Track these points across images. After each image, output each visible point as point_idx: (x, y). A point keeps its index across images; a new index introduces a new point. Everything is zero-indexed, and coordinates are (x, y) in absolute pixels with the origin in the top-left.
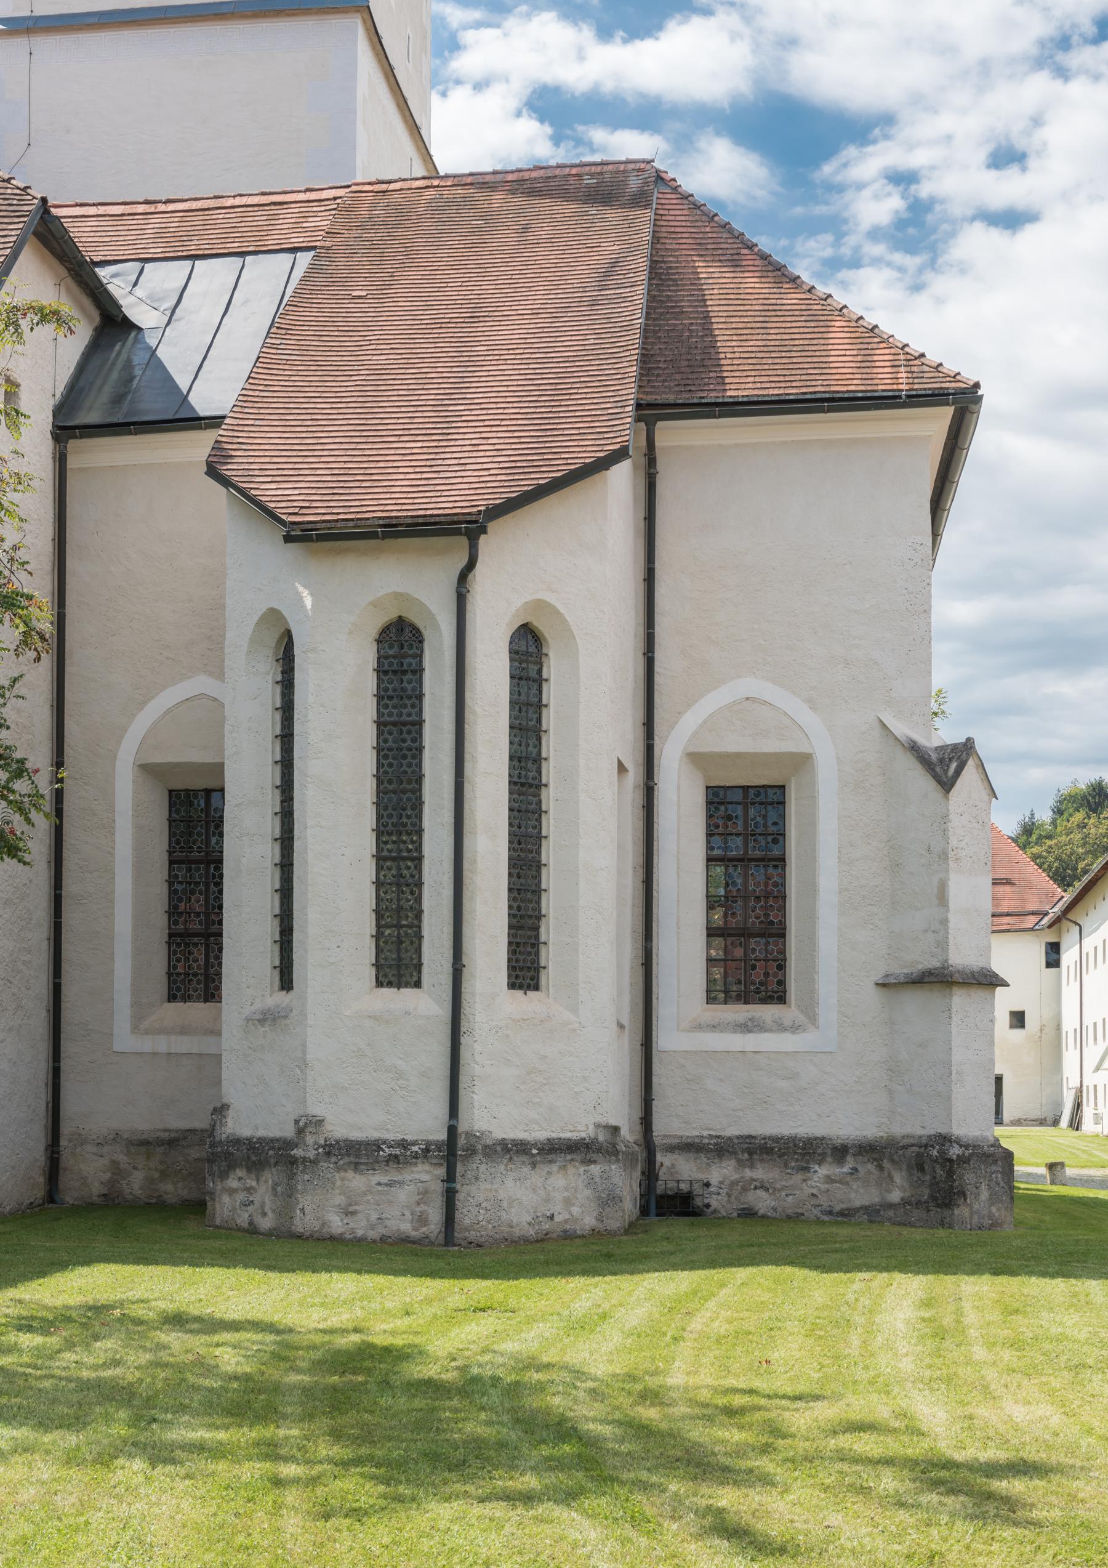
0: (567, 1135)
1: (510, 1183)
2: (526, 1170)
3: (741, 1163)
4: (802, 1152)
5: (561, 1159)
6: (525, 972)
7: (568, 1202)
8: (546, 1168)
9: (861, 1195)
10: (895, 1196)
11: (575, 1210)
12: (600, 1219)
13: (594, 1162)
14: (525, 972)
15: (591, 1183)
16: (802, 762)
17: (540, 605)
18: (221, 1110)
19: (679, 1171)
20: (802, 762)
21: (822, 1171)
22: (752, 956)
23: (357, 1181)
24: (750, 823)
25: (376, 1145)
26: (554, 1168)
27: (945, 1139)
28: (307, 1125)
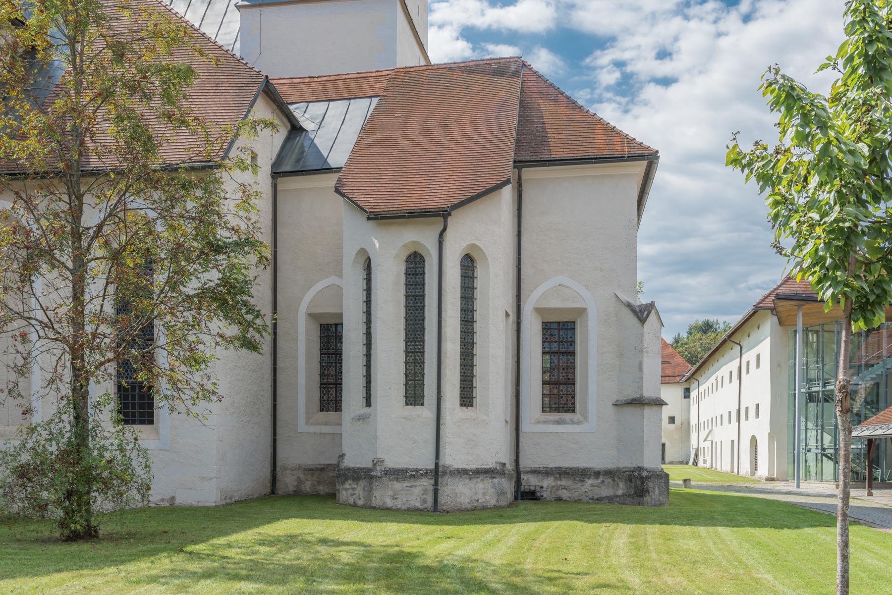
0: (484, 467)
1: (460, 486)
2: (467, 481)
3: (556, 479)
4: (581, 474)
5: (482, 476)
6: (467, 399)
7: (484, 494)
8: (475, 480)
9: (606, 492)
10: (620, 492)
11: (487, 498)
12: (497, 501)
13: (494, 478)
14: (467, 399)
15: (494, 486)
16: (582, 311)
17: (473, 246)
18: (342, 456)
19: (531, 482)
20: (582, 311)
21: (590, 482)
22: (561, 393)
23: (398, 485)
24: (561, 336)
25: (406, 471)
26: (479, 480)
27: (640, 469)
28: (377, 462)
